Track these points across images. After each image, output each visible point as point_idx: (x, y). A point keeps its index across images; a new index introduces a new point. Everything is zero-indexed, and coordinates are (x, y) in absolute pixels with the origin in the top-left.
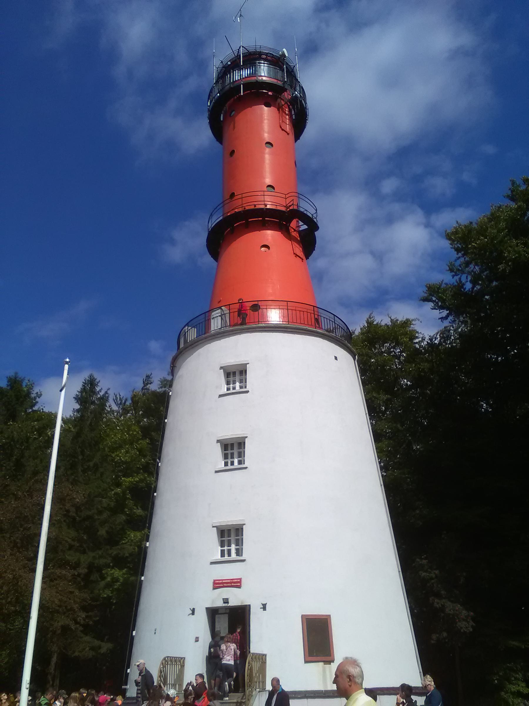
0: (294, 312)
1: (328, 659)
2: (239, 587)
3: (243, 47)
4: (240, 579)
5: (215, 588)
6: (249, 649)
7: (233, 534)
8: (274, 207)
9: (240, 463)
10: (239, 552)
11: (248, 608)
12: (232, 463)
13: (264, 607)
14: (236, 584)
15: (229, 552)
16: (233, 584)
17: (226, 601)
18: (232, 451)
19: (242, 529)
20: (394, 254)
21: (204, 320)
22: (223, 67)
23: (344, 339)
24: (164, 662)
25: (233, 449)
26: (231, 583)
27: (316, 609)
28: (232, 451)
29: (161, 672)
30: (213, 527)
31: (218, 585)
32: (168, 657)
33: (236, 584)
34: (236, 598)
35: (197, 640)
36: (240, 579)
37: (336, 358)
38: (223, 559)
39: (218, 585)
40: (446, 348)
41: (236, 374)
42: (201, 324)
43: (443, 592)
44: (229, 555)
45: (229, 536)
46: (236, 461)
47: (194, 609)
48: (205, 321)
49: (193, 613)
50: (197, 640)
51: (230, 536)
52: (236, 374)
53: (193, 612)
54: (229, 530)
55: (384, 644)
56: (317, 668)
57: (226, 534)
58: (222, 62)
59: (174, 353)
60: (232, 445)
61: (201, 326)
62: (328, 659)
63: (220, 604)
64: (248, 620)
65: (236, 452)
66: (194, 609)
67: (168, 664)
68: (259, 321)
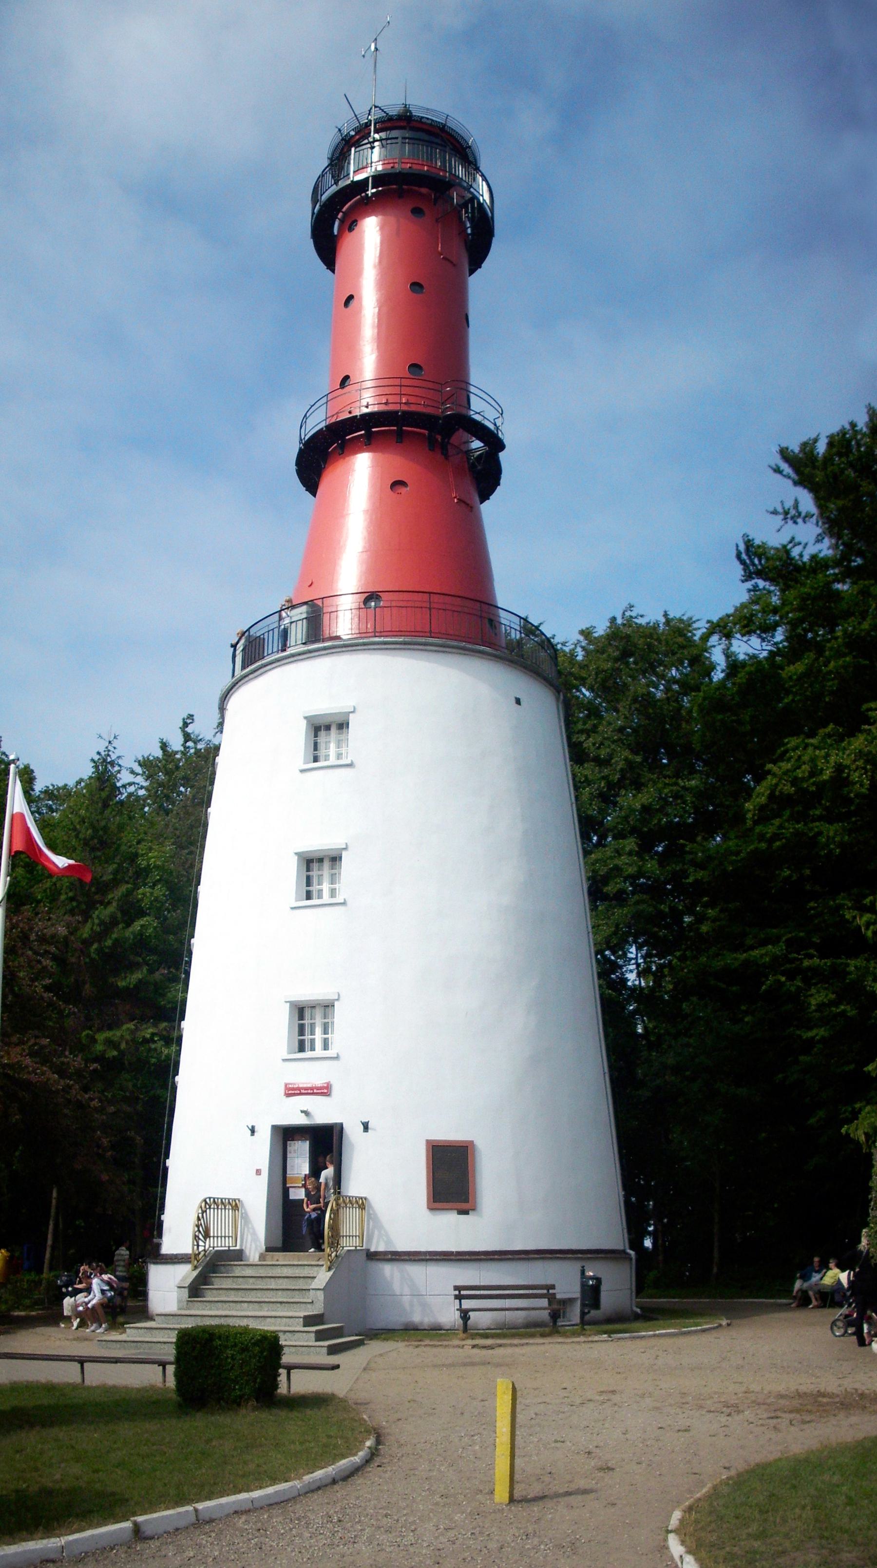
0: (395, 610)
3: (376, 107)
5: (288, 1095)
8: (383, 408)
9: (333, 893)
13: (366, 1127)
14: (325, 1091)
16: (303, 1091)
17: (306, 1113)
20: (876, 1189)
21: (276, 625)
22: (342, 139)
24: (203, 1204)
25: (317, 867)
26: (312, 1089)
28: (320, 873)
29: (199, 1219)
31: (292, 1091)
32: (210, 1198)
33: (325, 1091)
34: (323, 1113)
35: (258, 1172)
37: (518, 701)
39: (292, 1091)
42: (271, 632)
47: (253, 1127)
50: (258, 1172)
53: (253, 1131)
56: (449, 1219)
58: (340, 130)
59: (228, 681)
62: (464, 1206)
63: (301, 1120)
66: (253, 1127)
67: (210, 1208)
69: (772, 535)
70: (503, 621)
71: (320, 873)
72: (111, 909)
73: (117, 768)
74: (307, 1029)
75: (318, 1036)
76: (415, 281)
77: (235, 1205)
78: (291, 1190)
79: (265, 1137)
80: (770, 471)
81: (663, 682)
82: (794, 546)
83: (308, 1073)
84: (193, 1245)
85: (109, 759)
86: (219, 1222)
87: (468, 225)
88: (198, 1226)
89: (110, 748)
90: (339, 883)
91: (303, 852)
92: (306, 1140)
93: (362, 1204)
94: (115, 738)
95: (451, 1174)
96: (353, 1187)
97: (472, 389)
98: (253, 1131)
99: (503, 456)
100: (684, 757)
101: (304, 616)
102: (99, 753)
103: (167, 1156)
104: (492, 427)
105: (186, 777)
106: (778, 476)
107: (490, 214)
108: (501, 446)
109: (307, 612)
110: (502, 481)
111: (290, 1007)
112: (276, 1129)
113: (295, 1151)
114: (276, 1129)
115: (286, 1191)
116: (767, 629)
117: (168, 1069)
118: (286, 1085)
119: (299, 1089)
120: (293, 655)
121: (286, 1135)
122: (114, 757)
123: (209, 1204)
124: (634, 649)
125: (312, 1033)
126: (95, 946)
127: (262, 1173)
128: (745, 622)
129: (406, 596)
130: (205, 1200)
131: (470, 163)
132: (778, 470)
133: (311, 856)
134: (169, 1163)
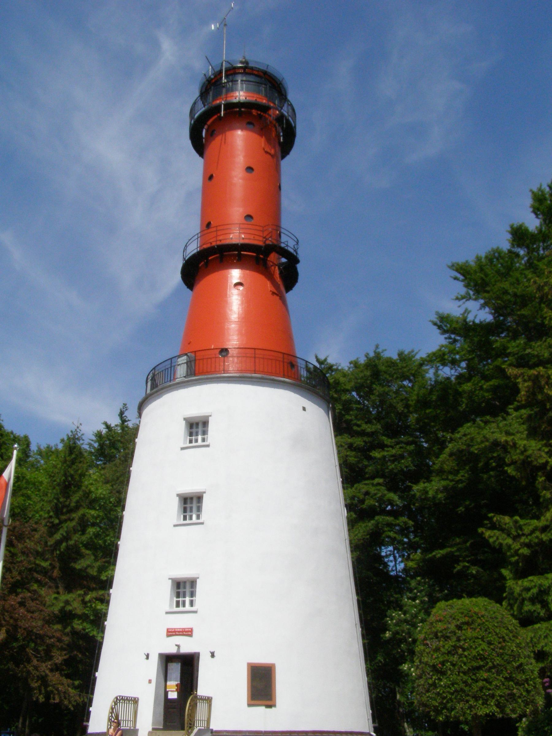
1: (269, 703)
2: (191, 635)
4: (192, 629)
6: (197, 691)
7: (188, 585)
9: (203, 440)
10: (198, 517)
11: (196, 658)
12: (196, 441)
13: (213, 655)
14: (188, 633)
15: (184, 602)
16: (177, 633)
18: (191, 505)
19: (196, 581)
21: (170, 366)
23: (319, 383)
25: (190, 504)
26: (182, 632)
27: (261, 658)
29: (112, 709)
30: (169, 579)
31: (171, 633)
32: (120, 696)
33: (188, 633)
34: (187, 646)
35: (150, 681)
36: (192, 629)
38: (185, 522)
39: (171, 633)
40: (511, 516)
41: (197, 427)
43: (394, 621)
44: (184, 605)
45: (191, 503)
46: (194, 517)
48: (171, 367)
49: (189, 344)
50: (150, 681)
51: (183, 588)
52: (197, 427)
54: (185, 582)
55: (327, 681)
57: (181, 586)
60: (197, 424)
61: (167, 372)
62: (269, 703)
63: (173, 650)
64: (195, 682)
65: (194, 506)
67: (120, 703)
68: (224, 371)
69: (454, 309)
70: (299, 365)
71: (191, 514)
72: (74, 523)
73: (81, 442)
74: (188, 510)
75: (187, 599)
76: (250, 214)
77: (135, 701)
78: (169, 693)
79: (154, 660)
80: (452, 280)
81: (388, 619)
82: (468, 314)
83: (180, 621)
84: (108, 725)
85: (77, 437)
86: (125, 713)
87: (281, 134)
88: (111, 713)
89: (78, 430)
90: (207, 434)
91: (175, 578)
92: (179, 662)
93: (208, 700)
94: (81, 424)
95: (262, 684)
96: (202, 690)
97: (282, 230)
98: (147, 657)
99: (299, 267)
100: (405, 525)
101: (185, 361)
102: (72, 432)
103: (96, 670)
104: (292, 251)
105: (117, 448)
106: (456, 281)
107: (293, 125)
108: (297, 261)
109: (187, 359)
110: (299, 280)
111: (173, 585)
112: (161, 656)
113: (172, 669)
114: (161, 656)
115: (166, 693)
116: (454, 363)
117: (99, 620)
118: (168, 629)
119: (175, 632)
120: (178, 383)
121: (167, 660)
122: (79, 435)
123: (119, 700)
124: (376, 372)
125: (185, 588)
126: (64, 544)
127: (152, 681)
128: (440, 358)
129: (244, 350)
130: (117, 698)
131: (282, 95)
132: (456, 279)
133: (186, 496)
134: (97, 674)
